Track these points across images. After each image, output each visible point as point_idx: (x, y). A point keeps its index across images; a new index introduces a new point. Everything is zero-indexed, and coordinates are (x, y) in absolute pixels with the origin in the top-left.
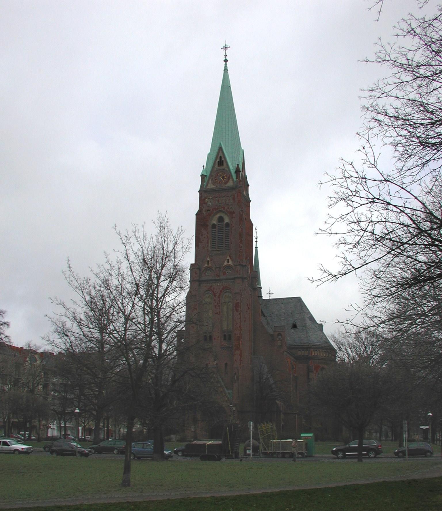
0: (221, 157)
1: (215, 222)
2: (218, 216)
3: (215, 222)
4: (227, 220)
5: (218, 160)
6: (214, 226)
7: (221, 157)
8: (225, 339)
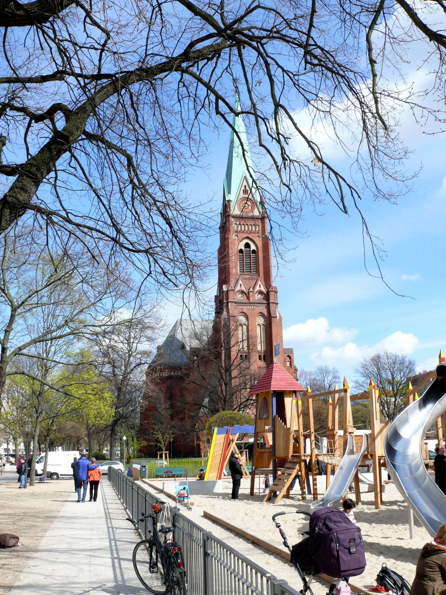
0: (245, 186)
1: (242, 246)
2: (246, 241)
3: (243, 248)
4: (253, 247)
5: (243, 188)
6: (241, 251)
7: (245, 186)
8: (260, 359)
